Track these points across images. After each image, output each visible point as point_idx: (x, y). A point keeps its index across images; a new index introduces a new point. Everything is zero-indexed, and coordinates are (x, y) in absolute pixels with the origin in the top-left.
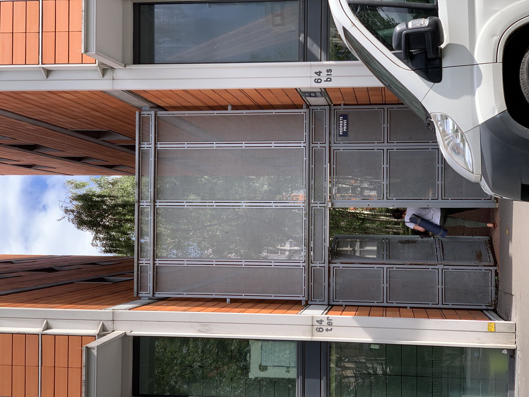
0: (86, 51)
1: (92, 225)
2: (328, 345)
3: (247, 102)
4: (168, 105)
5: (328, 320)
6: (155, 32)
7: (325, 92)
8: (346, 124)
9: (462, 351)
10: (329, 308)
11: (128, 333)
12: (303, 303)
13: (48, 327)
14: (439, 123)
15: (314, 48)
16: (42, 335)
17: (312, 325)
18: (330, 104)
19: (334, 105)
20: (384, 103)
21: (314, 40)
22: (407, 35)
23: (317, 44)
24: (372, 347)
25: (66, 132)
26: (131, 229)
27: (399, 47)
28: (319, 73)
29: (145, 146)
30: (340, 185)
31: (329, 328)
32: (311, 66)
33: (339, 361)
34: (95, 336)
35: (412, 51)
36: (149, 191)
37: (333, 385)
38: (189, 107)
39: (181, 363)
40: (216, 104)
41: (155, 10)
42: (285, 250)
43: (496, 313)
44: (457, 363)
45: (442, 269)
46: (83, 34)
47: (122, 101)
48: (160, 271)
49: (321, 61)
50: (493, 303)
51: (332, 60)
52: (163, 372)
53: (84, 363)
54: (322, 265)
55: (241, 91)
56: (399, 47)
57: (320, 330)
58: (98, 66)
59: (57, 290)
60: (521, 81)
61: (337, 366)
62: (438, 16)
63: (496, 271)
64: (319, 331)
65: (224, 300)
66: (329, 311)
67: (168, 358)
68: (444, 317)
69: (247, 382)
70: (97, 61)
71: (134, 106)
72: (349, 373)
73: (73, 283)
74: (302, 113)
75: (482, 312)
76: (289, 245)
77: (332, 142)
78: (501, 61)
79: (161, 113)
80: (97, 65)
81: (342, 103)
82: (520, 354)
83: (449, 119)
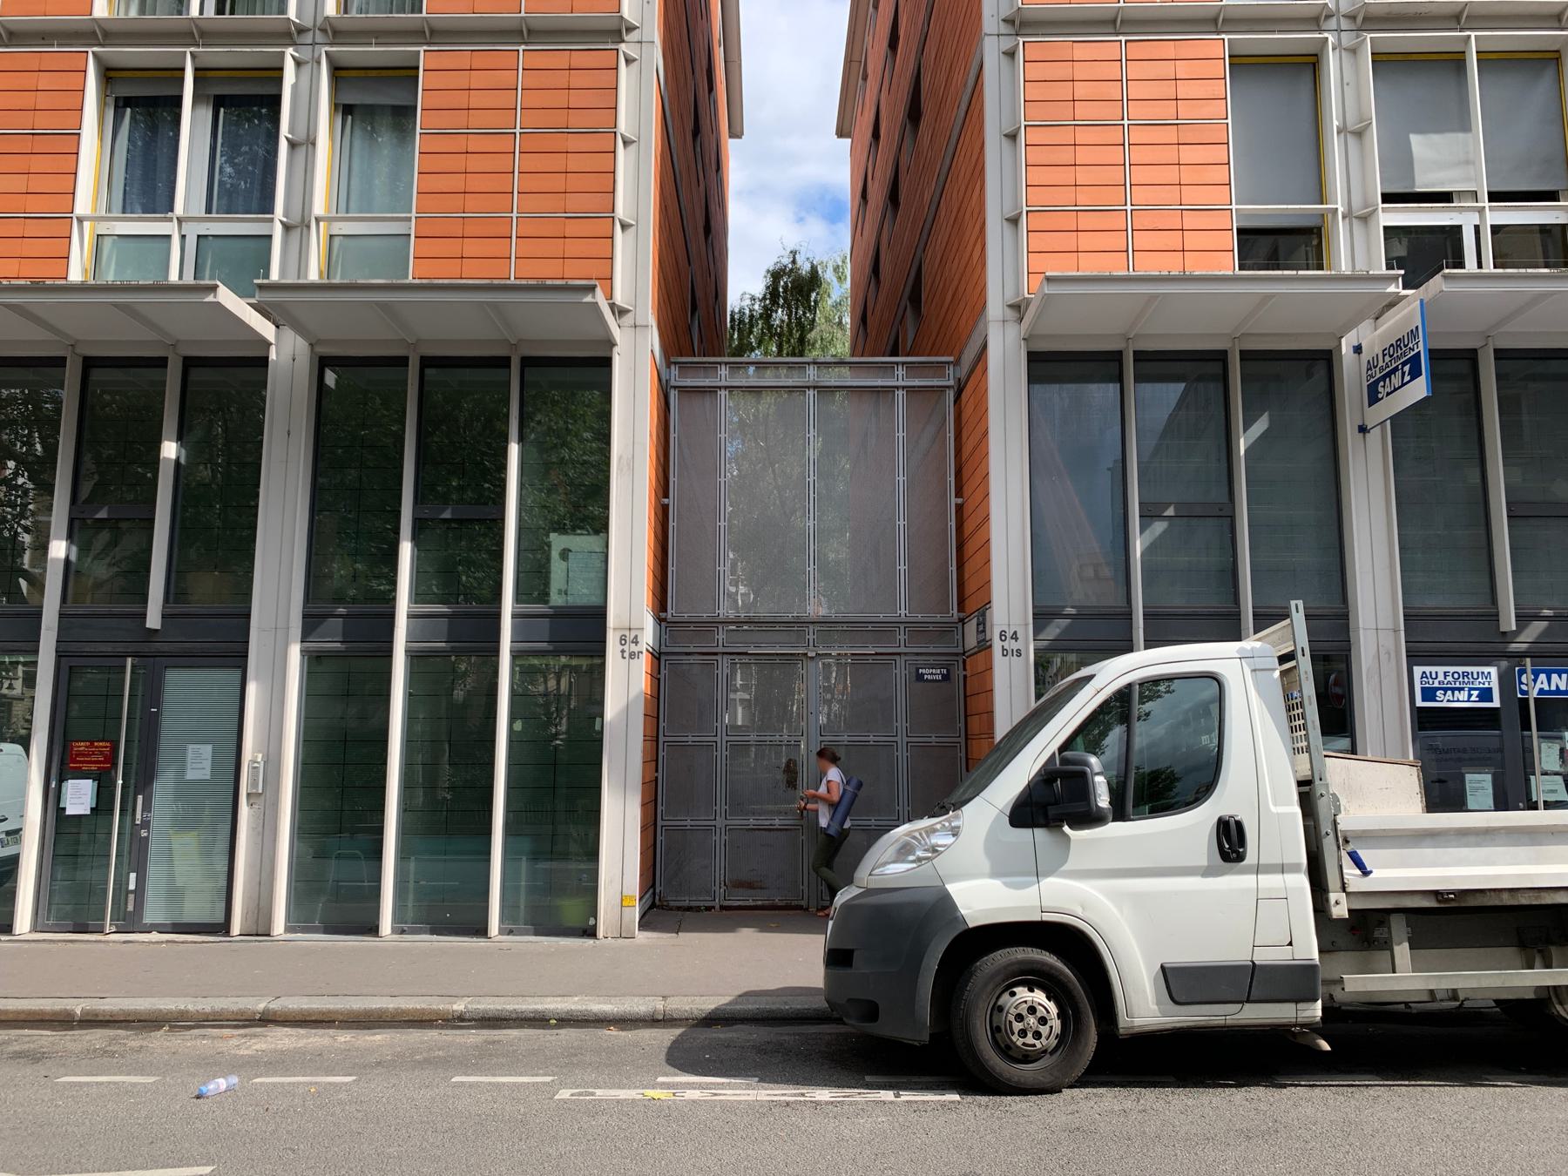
0: (1049, 279)
1: (773, 293)
2: (602, 654)
3: (969, 527)
4: (963, 407)
5: (639, 652)
6: (1078, 385)
7: (985, 646)
9: (593, 854)
10: (655, 653)
11: (616, 350)
12: (663, 615)
13: (624, 226)
14: (947, 824)
15: (1054, 630)
16: (613, 217)
17: (630, 629)
18: (966, 654)
19: (964, 661)
20: (969, 737)
21: (1067, 629)
22: (1083, 775)
23: (1060, 634)
24: (598, 720)
25: (919, 251)
26: (766, 353)
27: (1064, 761)
28: (1015, 637)
29: (900, 372)
30: (835, 668)
31: (626, 655)
32: (1026, 625)
33: (575, 670)
34: (611, 299)
35: (1059, 782)
36: (832, 378)
37: (536, 662)
38: (961, 438)
39: (567, 429)
40: (965, 479)
41: (1111, 385)
42: (737, 587)
43: (651, 908)
44: (573, 848)
45: (715, 826)
46: (1074, 273)
47: (969, 336)
48: (708, 399)
49: (1034, 640)
50: (665, 903)
51: (1035, 656)
52: (554, 403)
53: (571, 282)
54: (720, 644)
55: (987, 518)
56: (1064, 761)
57: (623, 640)
58: (1024, 298)
59: (680, 242)
60: (1014, 949)
61: (565, 667)
62: (1113, 821)
63: (714, 907)
64: (621, 640)
65: (666, 495)
66: (651, 653)
67: (576, 410)
68: (644, 829)
69: (541, 530)
70: (1033, 296)
71: (961, 353)
72: (552, 684)
73: (690, 264)
74: (951, 612)
75: (651, 887)
76: (743, 591)
77: (907, 658)
78: (1044, 919)
79: (951, 395)
80: (1027, 296)
81: (968, 673)
82: (589, 945)
83: (954, 839)
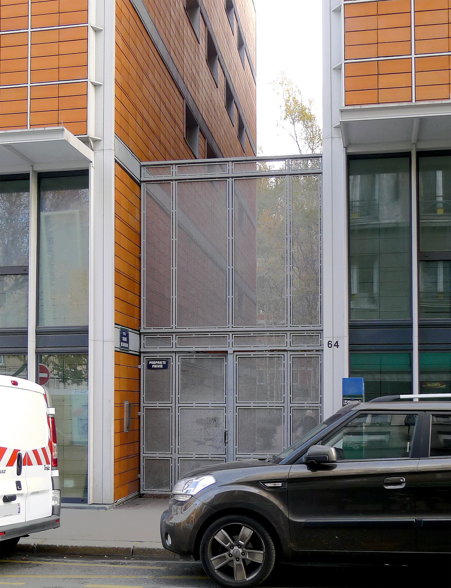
8: (158, 367)
